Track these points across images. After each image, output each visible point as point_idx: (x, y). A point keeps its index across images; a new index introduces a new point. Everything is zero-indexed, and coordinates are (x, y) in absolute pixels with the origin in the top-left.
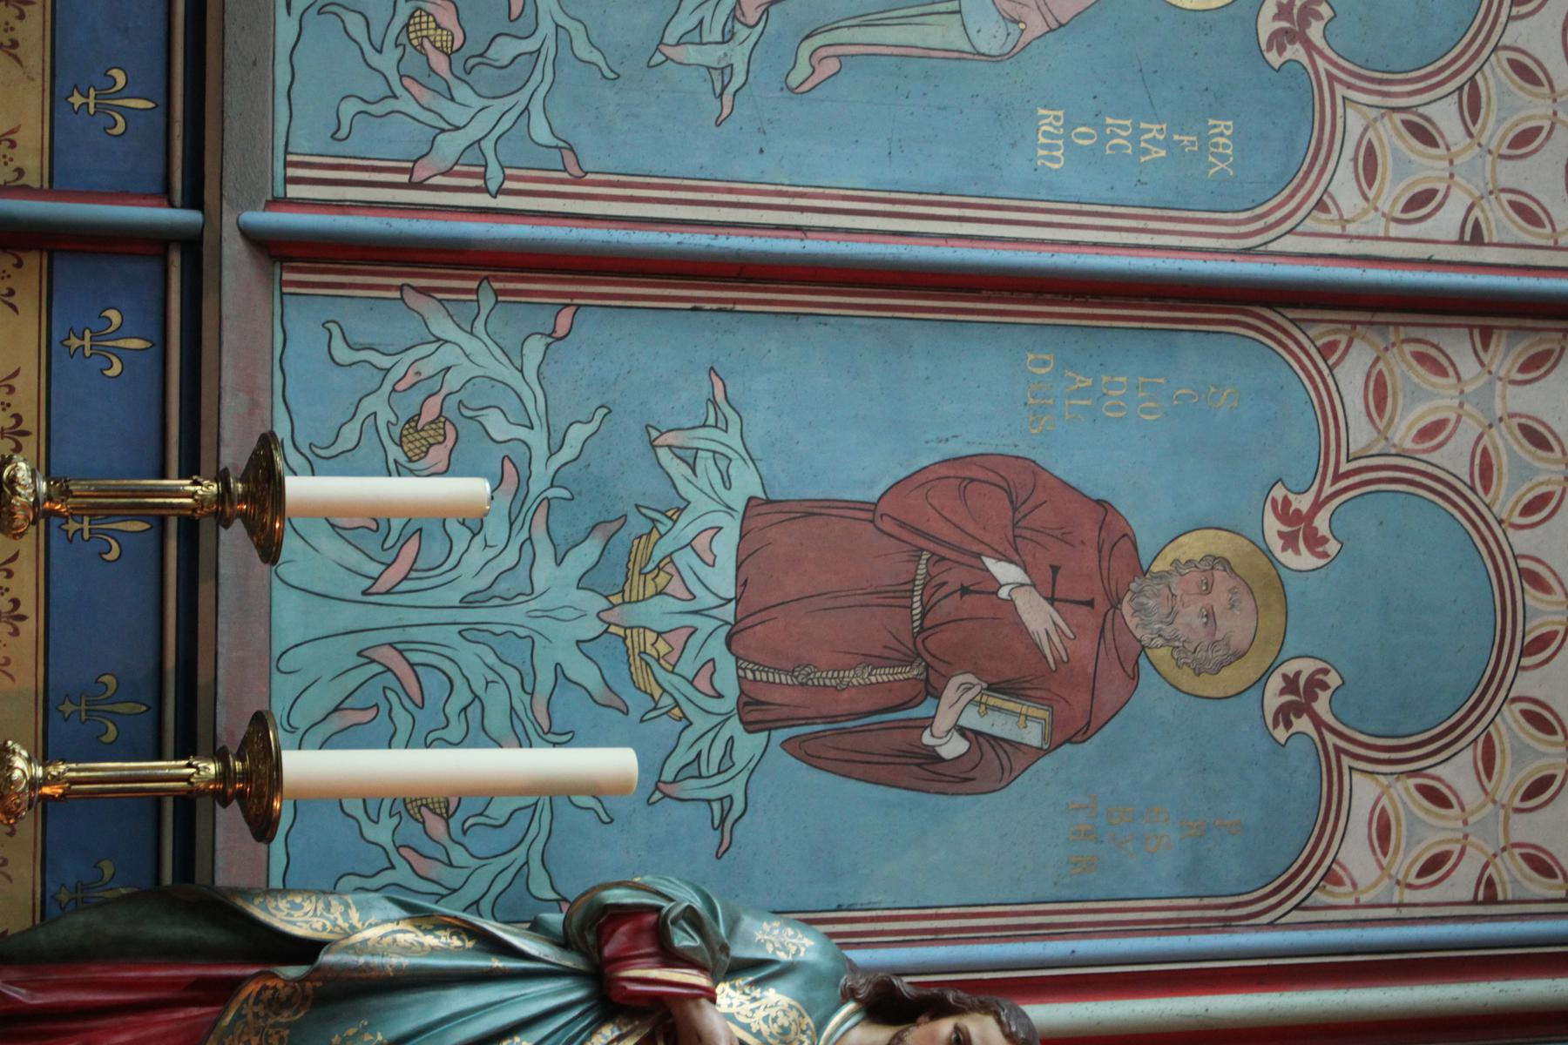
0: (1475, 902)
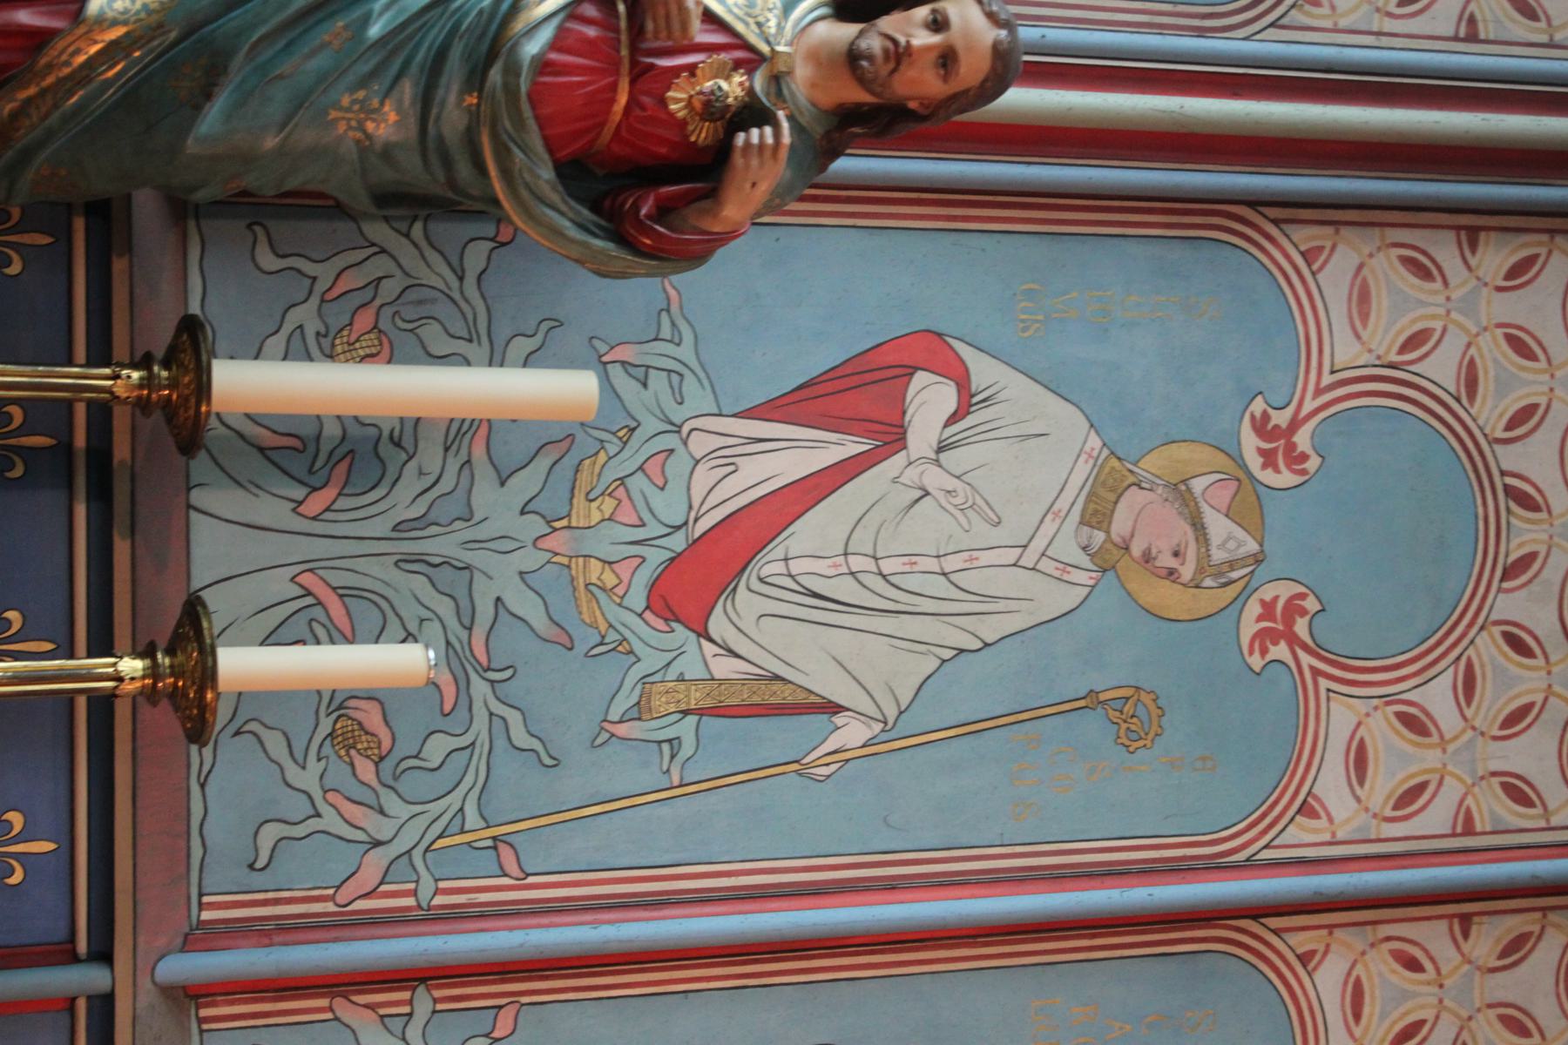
0: (1456, 39)
